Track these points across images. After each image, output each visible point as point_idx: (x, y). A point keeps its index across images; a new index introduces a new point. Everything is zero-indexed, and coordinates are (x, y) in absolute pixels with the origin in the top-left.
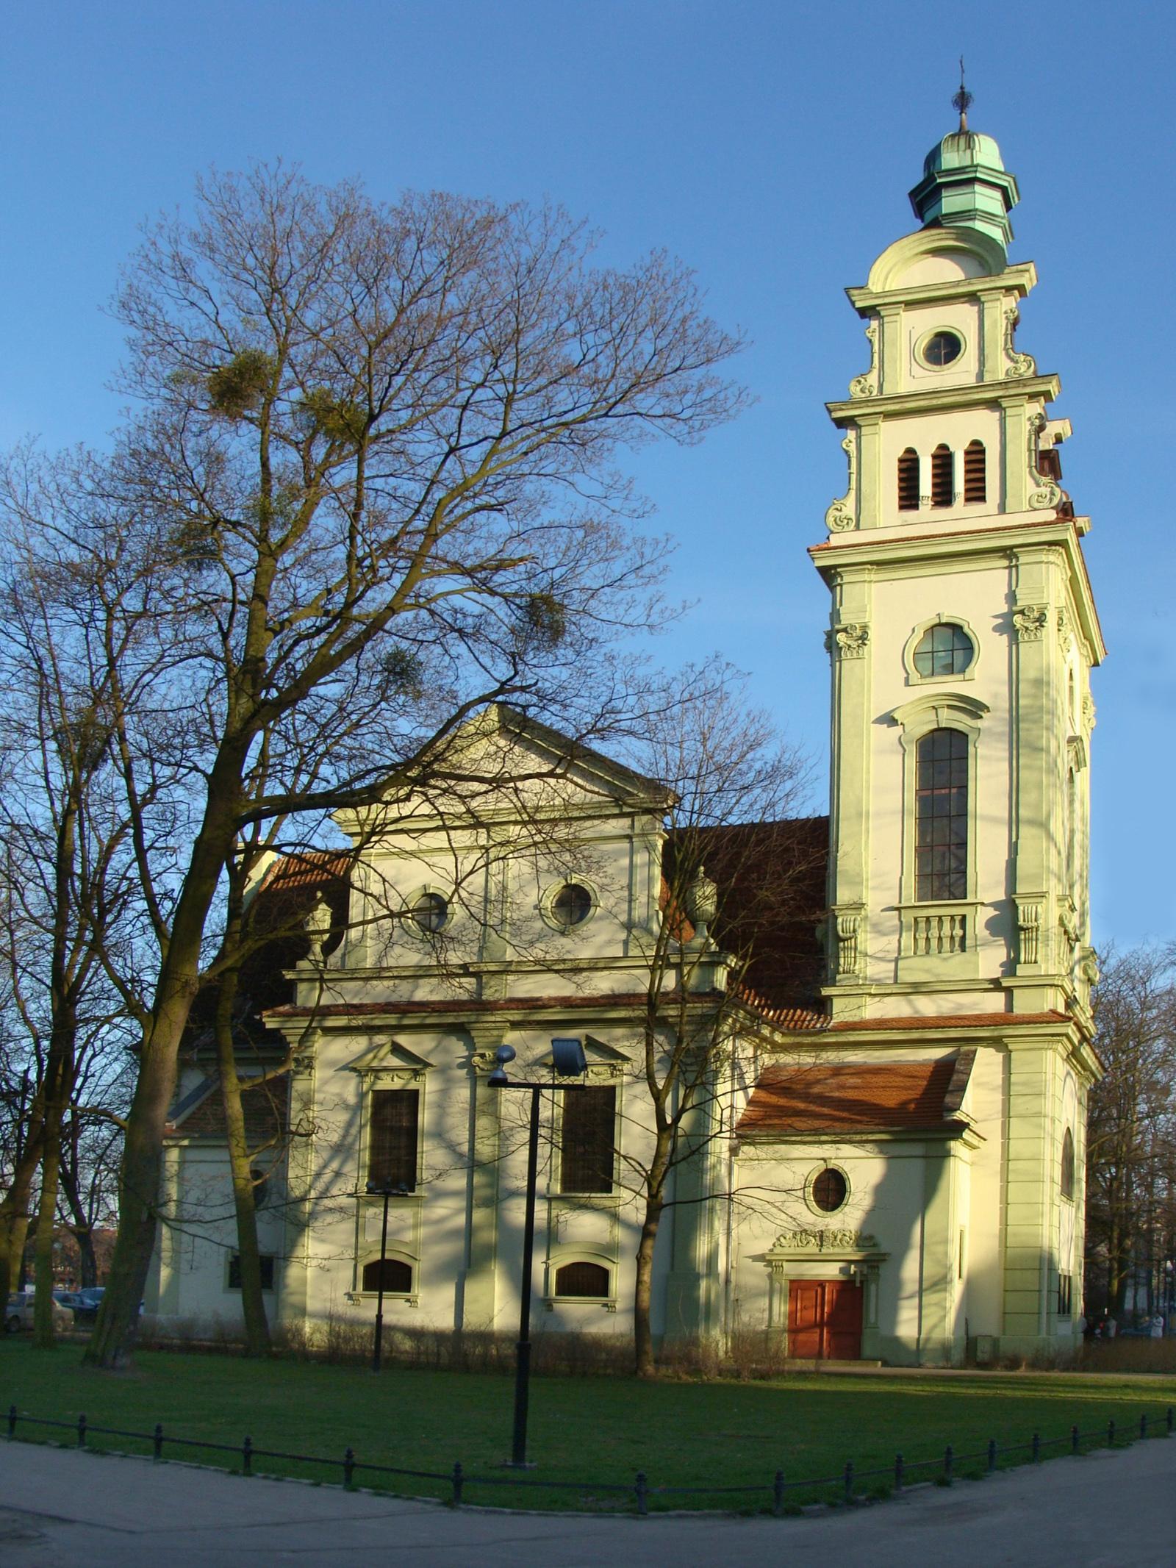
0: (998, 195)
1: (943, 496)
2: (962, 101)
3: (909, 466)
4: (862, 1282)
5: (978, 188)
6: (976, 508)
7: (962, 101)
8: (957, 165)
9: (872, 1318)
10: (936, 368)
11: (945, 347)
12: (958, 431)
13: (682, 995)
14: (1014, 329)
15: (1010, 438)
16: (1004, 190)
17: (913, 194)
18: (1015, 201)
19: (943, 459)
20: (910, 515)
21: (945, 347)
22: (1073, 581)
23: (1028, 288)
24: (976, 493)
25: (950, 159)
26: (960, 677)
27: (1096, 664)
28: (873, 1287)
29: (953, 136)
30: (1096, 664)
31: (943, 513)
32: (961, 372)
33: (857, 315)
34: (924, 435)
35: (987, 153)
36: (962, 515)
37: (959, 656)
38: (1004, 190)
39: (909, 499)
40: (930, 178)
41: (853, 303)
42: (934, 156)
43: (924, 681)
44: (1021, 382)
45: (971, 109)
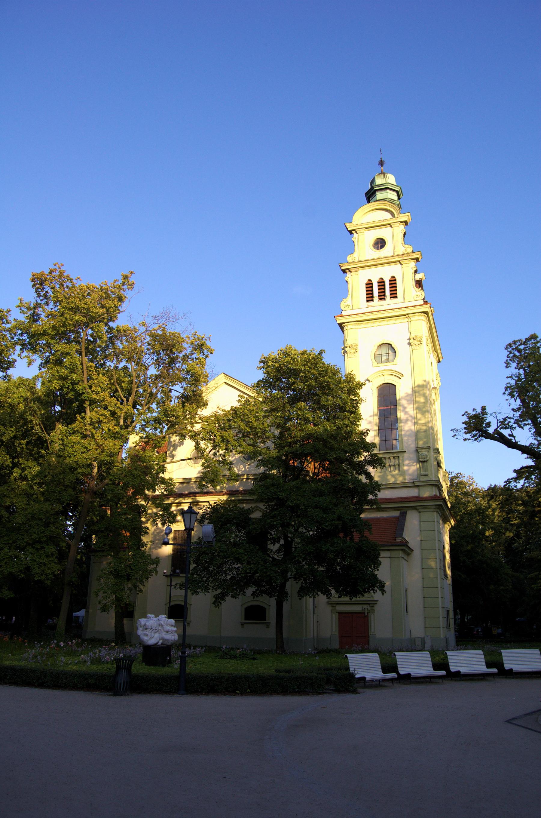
0: (395, 194)
1: (382, 297)
2: (381, 163)
3: (369, 286)
4: (368, 613)
5: (388, 191)
6: (394, 300)
7: (381, 163)
8: (381, 183)
9: (373, 630)
10: (378, 251)
11: (380, 243)
12: (386, 273)
13: (66, 413)
14: (404, 237)
15: (405, 276)
16: (397, 192)
17: (366, 194)
18: (401, 196)
19: (381, 283)
20: (370, 303)
21: (380, 243)
22: (430, 328)
23: (408, 222)
24: (394, 295)
25: (379, 181)
26: (392, 363)
27: (439, 361)
28: (372, 616)
29: (379, 174)
30: (439, 361)
31: (382, 302)
32: (386, 251)
33: (342, 272)
34: (374, 275)
35: (391, 179)
36: (389, 302)
37: (391, 356)
38: (397, 192)
39: (370, 298)
40: (372, 188)
41: (347, 229)
42: (373, 181)
43: (378, 365)
44: (408, 254)
45: (385, 166)
